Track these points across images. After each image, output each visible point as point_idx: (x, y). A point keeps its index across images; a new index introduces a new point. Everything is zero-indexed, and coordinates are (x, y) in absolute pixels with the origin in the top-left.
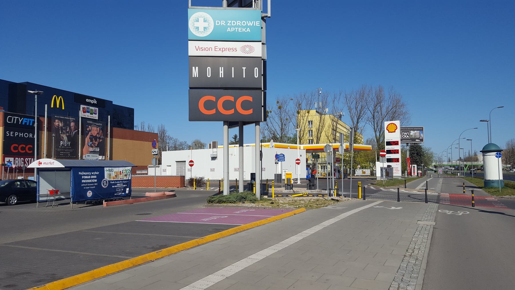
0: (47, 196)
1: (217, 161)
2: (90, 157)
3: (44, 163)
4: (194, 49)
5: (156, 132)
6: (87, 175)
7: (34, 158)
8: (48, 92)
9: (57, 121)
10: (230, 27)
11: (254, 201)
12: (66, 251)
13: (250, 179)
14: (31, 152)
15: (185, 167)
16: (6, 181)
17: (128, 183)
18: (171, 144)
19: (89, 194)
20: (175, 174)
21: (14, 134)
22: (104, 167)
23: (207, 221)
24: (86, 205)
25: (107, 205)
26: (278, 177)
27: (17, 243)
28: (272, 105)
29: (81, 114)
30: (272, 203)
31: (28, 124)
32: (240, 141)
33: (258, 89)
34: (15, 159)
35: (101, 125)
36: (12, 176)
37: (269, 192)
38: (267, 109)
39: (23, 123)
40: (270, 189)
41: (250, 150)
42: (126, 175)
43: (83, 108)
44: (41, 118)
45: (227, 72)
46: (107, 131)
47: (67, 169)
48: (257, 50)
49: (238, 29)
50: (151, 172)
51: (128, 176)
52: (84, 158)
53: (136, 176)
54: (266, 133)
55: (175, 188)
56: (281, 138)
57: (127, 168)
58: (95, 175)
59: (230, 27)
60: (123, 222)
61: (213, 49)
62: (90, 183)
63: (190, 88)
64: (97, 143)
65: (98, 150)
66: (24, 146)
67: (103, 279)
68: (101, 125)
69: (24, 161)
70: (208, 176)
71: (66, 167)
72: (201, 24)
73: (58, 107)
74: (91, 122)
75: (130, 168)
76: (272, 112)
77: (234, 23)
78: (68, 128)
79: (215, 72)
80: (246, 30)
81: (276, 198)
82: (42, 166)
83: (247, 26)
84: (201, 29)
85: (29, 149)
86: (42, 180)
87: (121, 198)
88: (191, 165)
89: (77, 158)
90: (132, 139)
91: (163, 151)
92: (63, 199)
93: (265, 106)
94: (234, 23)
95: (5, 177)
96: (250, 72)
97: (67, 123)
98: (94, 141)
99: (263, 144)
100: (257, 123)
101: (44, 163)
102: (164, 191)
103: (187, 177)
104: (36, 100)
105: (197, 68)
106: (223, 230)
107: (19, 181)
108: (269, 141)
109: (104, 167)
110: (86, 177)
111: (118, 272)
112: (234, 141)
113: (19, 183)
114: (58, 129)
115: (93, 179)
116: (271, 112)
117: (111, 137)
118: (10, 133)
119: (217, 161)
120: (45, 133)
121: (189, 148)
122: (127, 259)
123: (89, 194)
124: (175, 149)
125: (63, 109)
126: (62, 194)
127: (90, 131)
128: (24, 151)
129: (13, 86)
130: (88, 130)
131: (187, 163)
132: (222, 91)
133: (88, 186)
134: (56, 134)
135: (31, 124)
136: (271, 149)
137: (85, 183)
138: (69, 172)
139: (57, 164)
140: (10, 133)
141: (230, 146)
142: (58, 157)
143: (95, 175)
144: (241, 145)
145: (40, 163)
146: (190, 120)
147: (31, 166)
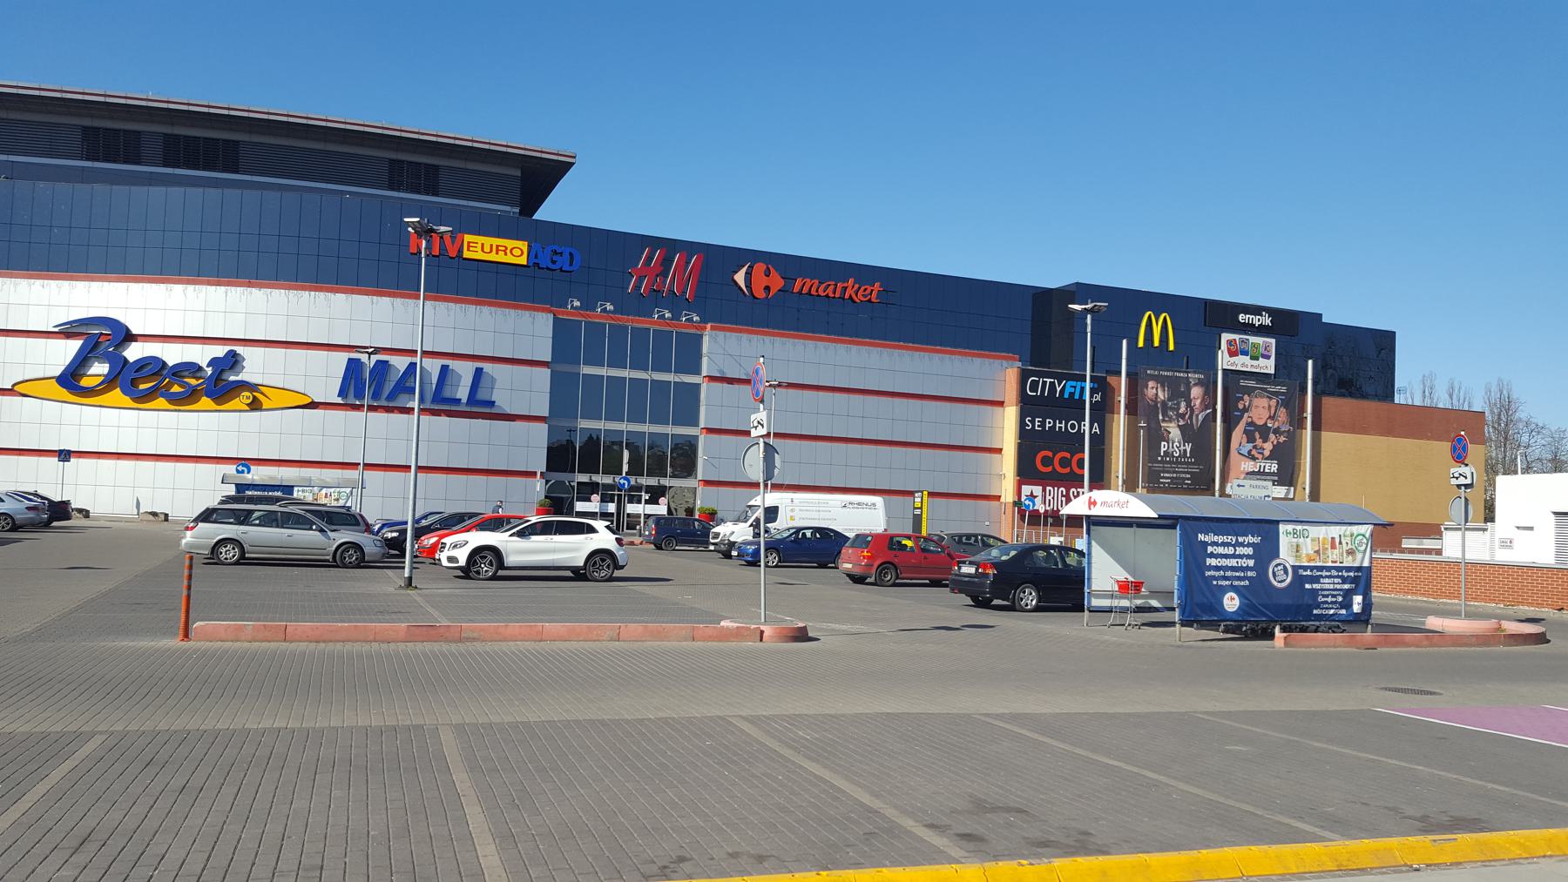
0: (1112, 597)
2: (1247, 488)
3: (1104, 503)
6: (1224, 544)
8: (1124, 307)
9: (1151, 384)
12: (1136, 770)
16: (1013, 547)
17: (1361, 580)
21: (1043, 424)
22: (1278, 522)
24: (1222, 635)
25: (1286, 644)
27: (1015, 718)
29: (1224, 361)
35: (1284, 389)
36: (1038, 535)
42: (1351, 552)
43: (1229, 342)
46: (1303, 409)
47: (1166, 522)
50: (1450, 545)
51: (1359, 556)
52: (1228, 490)
53: (1396, 556)
55: (1546, 612)
58: (1249, 545)
62: (1233, 569)
64: (1268, 447)
65: (1274, 468)
66: (1050, 454)
68: (1284, 389)
73: (1156, 343)
74: (1252, 383)
75: (1366, 530)
78: (1183, 404)
82: (1098, 511)
85: (1065, 463)
86: (1096, 548)
90: (1389, 431)
92: (1156, 610)
98: (1259, 442)
101: (1104, 503)
102: (1500, 618)
109: (1278, 522)
110: (1220, 550)
114: (1153, 409)
115: (1241, 556)
117: (1317, 427)
118: (1033, 422)
122: (1316, 839)
123: (1231, 602)
125: (1171, 347)
126: (1154, 594)
127: (1246, 410)
128: (1050, 469)
133: (1225, 578)
134: (1147, 422)
137: (1217, 568)
140: (1033, 422)
142: (1154, 485)
143: (1249, 545)
145: (1092, 503)
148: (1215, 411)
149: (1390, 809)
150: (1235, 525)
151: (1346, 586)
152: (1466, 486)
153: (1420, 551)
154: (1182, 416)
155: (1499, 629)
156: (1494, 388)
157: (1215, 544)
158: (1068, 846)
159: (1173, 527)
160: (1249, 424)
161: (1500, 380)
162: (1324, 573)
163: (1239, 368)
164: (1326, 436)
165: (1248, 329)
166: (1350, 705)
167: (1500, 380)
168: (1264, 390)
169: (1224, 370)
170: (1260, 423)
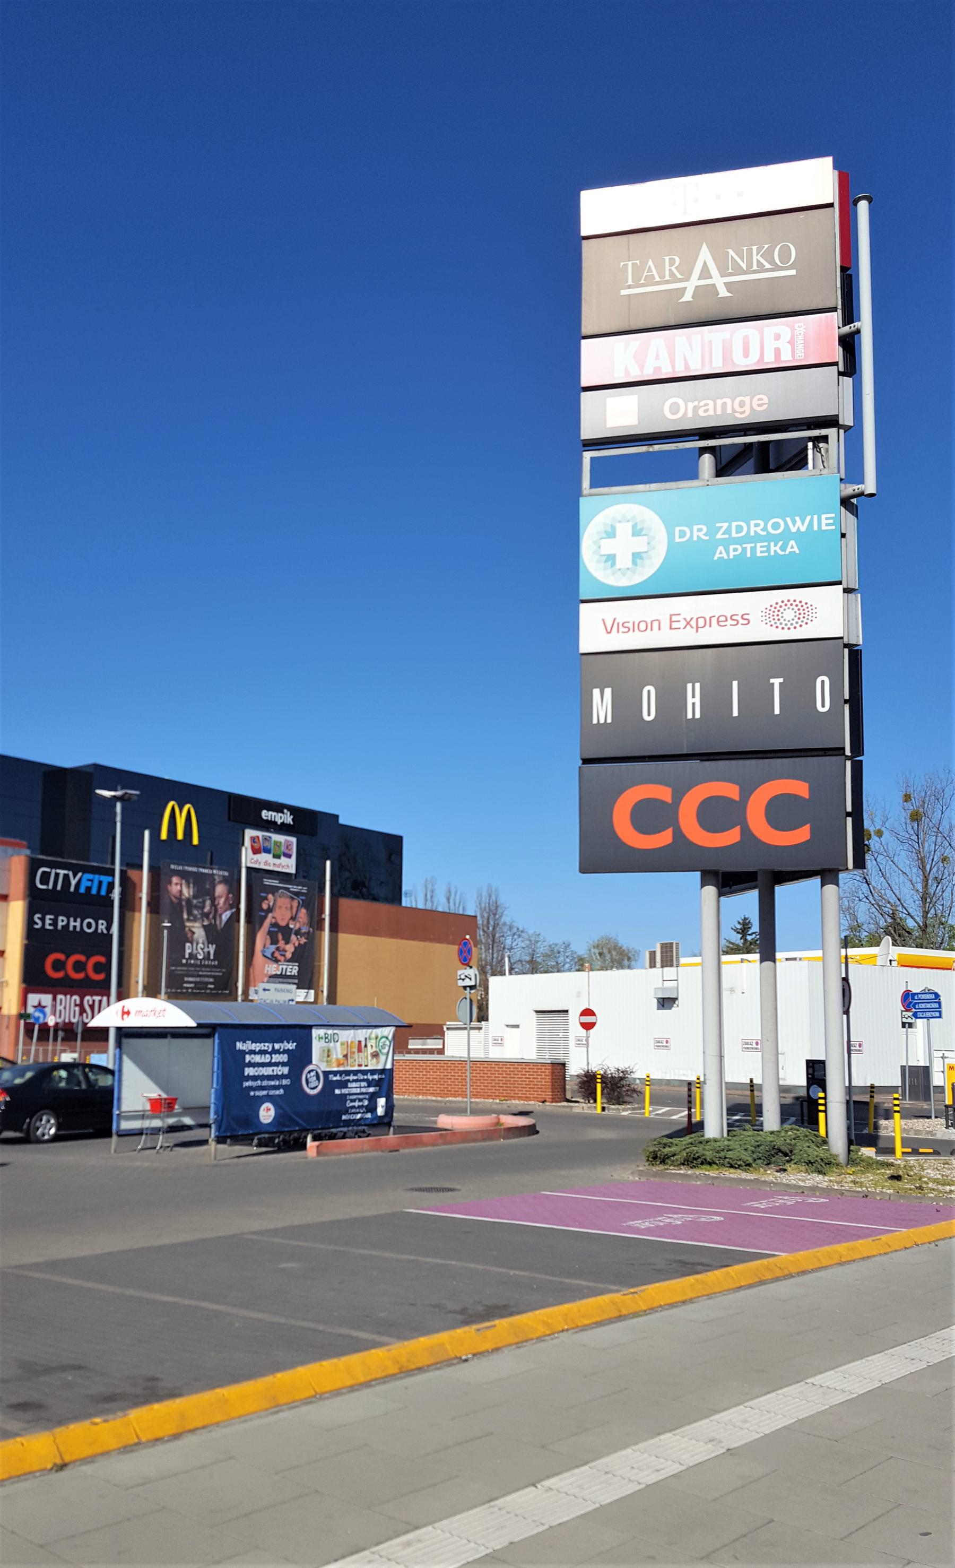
1: (684, 1010)
2: (271, 993)
4: (596, 630)
5: (470, 912)
6: (262, 1052)
7: (109, 996)
8: (153, 793)
9: (175, 880)
10: (726, 543)
11: (823, 1165)
13: (804, 1083)
14: (102, 976)
15: (566, 1031)
16: (28, 1068)
17: (384, 1082)
18: (518, 949)
19: (267, 1113)
20: (531, 1055)
21: (55, 923)
22: (310, 1027)
23: (648, 1231)
25: (319, 1153)
26: (918, 1079)
27: (53, 1266)
28: (883, 806)
29: (247, 858)
30: (898, 1178)
31: (94, 891)
32: (763, 942)
33: (837, 753)
34: (54, 999)
35: (304, 890)
36: (45, 1052)
37: (882, 1133)
38: (867, 824)
39: (82, 890)
40: (883, 1122)
41: (801, 972)
42: (375, 1055)
44: (132, 873)
45: (715, 699)
46: (322, 911)
47: (205, 1031)
48: (828, 614)
49: (753, 549)
50: (456, 1044)
51: (383, 1058)
53: (408, 1057)
54: (864, 911)
55: (533, 1105)
56: (924, 928)
57: (379, 1032)
59: (726, 543)
60: (368, 1213)
61: (665, 624)
63: (586, 761)
64: (290, 949)
65: (295, 971)
67: (304, 1409)
68: (304, 890)
69: (81, 1006)
70: (646, 1066)
71: (200, 1026)
72: (623, 546)
73: (180, 836)
74: (275, 883)
75: (389, 1032)
76: (886, 834)
77: (739, 530)
78: (208, 903)
79: (671, 701)
80: (783, 548)
81: (912, 1160)
82: (132, 1022)
83: (786, 536)
84: (624, 561)
85: (98, 968)
86: (128, 1065)
87: (362, 1129)
88: (588, 1026)
89: (232, 996)
90: (397, 932)
91: (493, 974)
92: (189, 1128)
93: (857, 814)
94: (739, 530)
95: (27, 1053)
96: (800, 694)
97: (203, 887)
98: (281, 943)
99: (851, 952)
100: (829, 875)
102: (499, 1112)
103: (575, 1068)
104: (119, 818)
105: (608, 692)
106: (708, 1267)
107: (65, 1066)
108: (874, 941)
109: (310, 1027)
110: (257, 1059)
111: (353, 1389)
112: (740, 942)
113: (63, 1074)
114: (177, 909)
116: (879, 834)
117: (334, 929)
118: (43, 920)
119: (684, 1010)
120: (142, 918)
121: (580, 965)
123: (267, 1113)
124: (534, 967)
125: (195, 841)
126: (187, 1110)
127: (270, 910)
129: (55, 778)
130: (265, 906)
131: (574, 1019)
132: (695, 763)
135: (103, 892)
136: (883, 973)
137: (255, 1078)
138: (208, 1041)
139: (172, 1015)
140: (43, 920)
141: (725, 958)
142: (177, 994)
143: (285, 1052)
144: (768, 955)
145: (126, 1013)
146: (583, 870)
147: (98, 1021)
148: (238, 910)
149: (434, 1306)
150: (272, 1032)
151: (371, 1090)
152: (471, 987)
153: (424, 1051)
154: (206, 915)
155: (498, 1123)
156: (485, 894)
157: (252, 1052)
158: (138, 1396)
159: (209, 1036)
160: (275, 925)
161: (490, 886)
162: (352, 1077)
163: (262, 866)
164: (343, 937)
165: (270, 826)
166: (384, 1209)
167: (490, 886)
168: (287, 889)
169: (248, 868)
170: (283, 923)
